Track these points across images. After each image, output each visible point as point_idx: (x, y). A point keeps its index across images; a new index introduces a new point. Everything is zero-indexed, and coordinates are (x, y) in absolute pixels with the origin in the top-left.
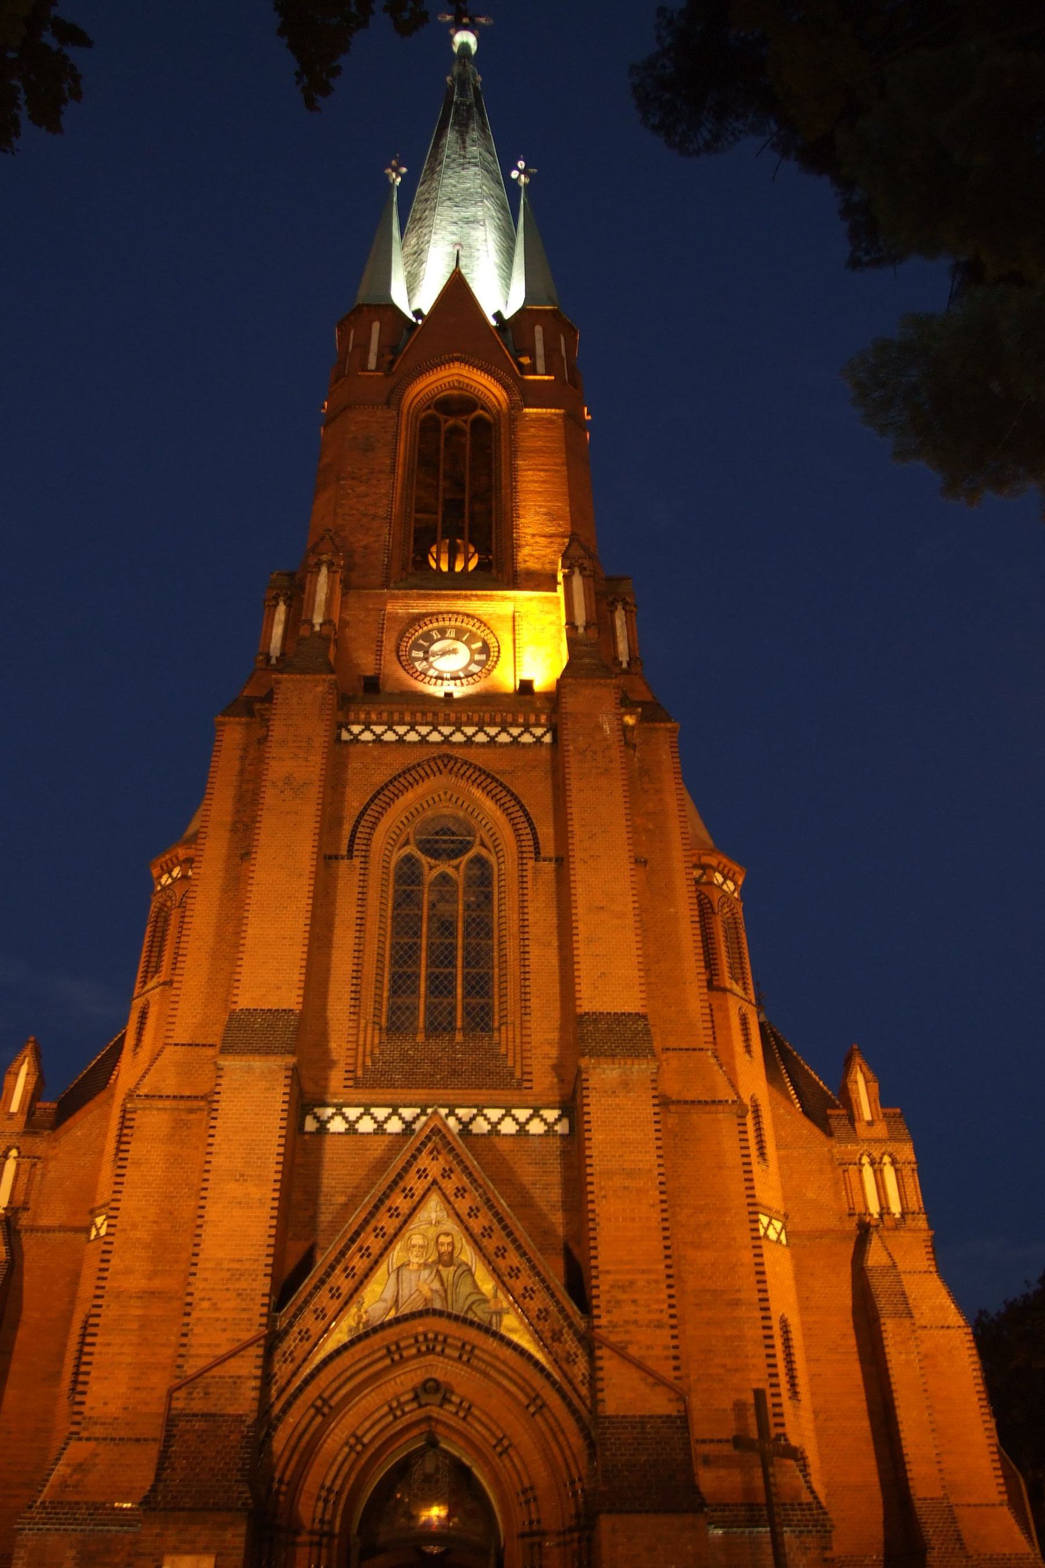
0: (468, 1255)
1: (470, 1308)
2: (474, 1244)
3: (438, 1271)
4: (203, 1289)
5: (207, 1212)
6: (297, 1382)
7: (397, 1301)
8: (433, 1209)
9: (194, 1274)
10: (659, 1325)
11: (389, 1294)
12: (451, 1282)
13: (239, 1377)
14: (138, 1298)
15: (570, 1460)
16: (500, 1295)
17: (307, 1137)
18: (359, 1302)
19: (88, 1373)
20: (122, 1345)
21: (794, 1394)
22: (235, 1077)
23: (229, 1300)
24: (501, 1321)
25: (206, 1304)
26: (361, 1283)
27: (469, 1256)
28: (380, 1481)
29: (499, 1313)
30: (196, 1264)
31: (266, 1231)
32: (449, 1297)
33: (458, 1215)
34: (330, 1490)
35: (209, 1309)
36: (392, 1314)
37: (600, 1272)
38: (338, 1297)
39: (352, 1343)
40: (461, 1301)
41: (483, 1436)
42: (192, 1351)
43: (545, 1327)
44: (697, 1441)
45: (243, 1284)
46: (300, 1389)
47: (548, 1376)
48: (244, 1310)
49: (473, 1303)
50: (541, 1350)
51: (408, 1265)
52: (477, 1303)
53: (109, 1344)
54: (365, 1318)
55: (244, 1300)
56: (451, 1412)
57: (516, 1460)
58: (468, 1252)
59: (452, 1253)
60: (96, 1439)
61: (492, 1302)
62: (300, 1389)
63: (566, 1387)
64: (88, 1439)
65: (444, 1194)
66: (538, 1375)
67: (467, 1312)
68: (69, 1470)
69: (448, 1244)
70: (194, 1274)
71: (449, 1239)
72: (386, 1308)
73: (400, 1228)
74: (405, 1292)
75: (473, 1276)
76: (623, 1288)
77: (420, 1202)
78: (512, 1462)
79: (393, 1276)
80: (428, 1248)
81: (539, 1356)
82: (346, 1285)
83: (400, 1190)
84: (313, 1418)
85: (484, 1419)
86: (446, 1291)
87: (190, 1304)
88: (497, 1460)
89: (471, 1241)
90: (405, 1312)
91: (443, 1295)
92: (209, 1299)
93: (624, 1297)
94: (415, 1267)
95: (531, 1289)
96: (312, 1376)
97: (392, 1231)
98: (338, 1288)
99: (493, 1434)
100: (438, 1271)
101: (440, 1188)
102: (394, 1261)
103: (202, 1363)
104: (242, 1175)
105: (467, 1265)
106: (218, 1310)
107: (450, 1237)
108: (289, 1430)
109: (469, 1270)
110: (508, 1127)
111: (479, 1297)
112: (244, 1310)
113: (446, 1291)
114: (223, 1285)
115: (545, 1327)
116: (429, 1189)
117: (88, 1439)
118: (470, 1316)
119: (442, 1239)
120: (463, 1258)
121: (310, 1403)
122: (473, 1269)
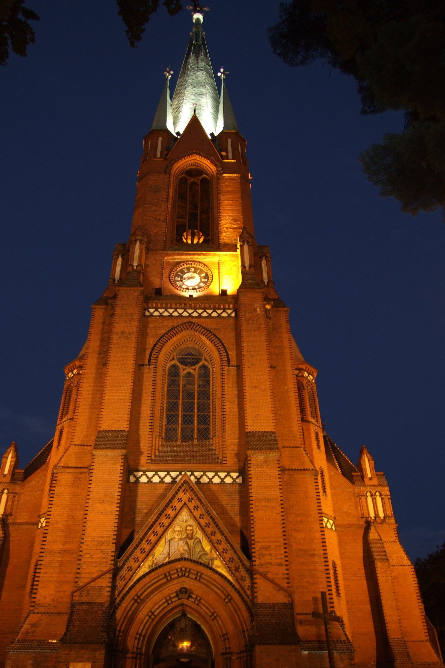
0: (199, 534)
1: (200, 557)
2: (202, 530)
3: (186, 542)
4: (87, 549)
5: (88, 516)
6: (127, 589)
7: (169, 554)
8: (184, 515)
9: (83, 543)
10: (281, 565)
11: (166, 551)
12: (192, 546)
13: (102, 587)
14: (59, 553)
15: (243, 622)
16: (213, 552)
17: (131, 484)
18: (153, 555)
19: (37, 585)
20: (52, 573)
21: (338, 594)
22: (100, 459)
23: (97, 554)
24: (213, 563)
25: (88, 556)
26: (154, 546)
27: (200, 535)
28: (162, 631)
29: (213, 559)
30: (83, 539)
31: (113, 525)
32: (191, 552)
33: (195, 518)
34: (140, 635)
35: (89, 558)
36: (167, 560)
37: (256, 542)
38: (144, 553)
39: (150, 572)
40: (196, 554)
41: (206, 612)
42: (82, 576)
43: (232, 565)
44: (297, 614)
45: (103, 547)
46: (128, 592)
47: (233, 586)
48: (104, 558)
49: (201, 555)
50: (230, 575)
51: (174, 539)
52: (203, 555)
53: (46, 573)
54: (155, 561)
55: (104, 554)
56: (192, 602)
57: (220, 622)
58: (199, 533)
59: (192, 534)
60: (41, 613)
61: (210, 555)
62: (128, 592)
63: (241, 591)
64: (37, 613)
65: (189, 509)
66: (229, 586)
67: (199, 559)
68: (29, 626)
69: (191, 530)
70: (83, 543)
71: (191, 528)
72: (164, 557)
73: (171, 523)
74: (172, 551)
75: (201, 543)
76: (265, 549)
77: (179, 512)
78: (218, 623)
79: (167, 544)
80: (182, 532)
81: (230, 578)
82: (147, 548)
83: (171, 507)
84: (133, 604)
85: (206, 604)
86: (190, 550)
87: (81, 556)
88: (212, 622)
89: (201, 529)
90: (172, 559)
91: (189, 552)
92: (89, 553)
93: (266, 552)
94: (177, 540)
95: (226, 549)
96: (133, 586)
97: (167, 525)
98: (144, 549)
99: (210, 611)
100: (186, 542)
101: (187, 506)
102: (168, 537)
103: (86, 581)
104: (103, 501)
105: (199, 539)
106: (93, 558)
107: (192, 527)
108: (123, 609)
109: (200, 541)
110: (216, 480)
111: (204, 552)
112: (104, 558)
113: (190, 550)
114: (95, 547)
115: (232, 565)
116: (183, 507)
117: (37, 613)
118: (200, 560)
119: (188, 528)
120: (197, 536)
121: (132, 598)
122: (202, 541)
